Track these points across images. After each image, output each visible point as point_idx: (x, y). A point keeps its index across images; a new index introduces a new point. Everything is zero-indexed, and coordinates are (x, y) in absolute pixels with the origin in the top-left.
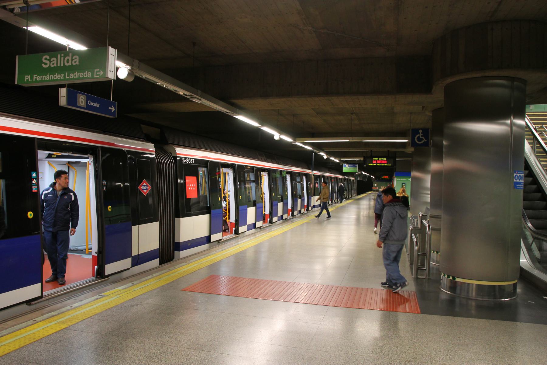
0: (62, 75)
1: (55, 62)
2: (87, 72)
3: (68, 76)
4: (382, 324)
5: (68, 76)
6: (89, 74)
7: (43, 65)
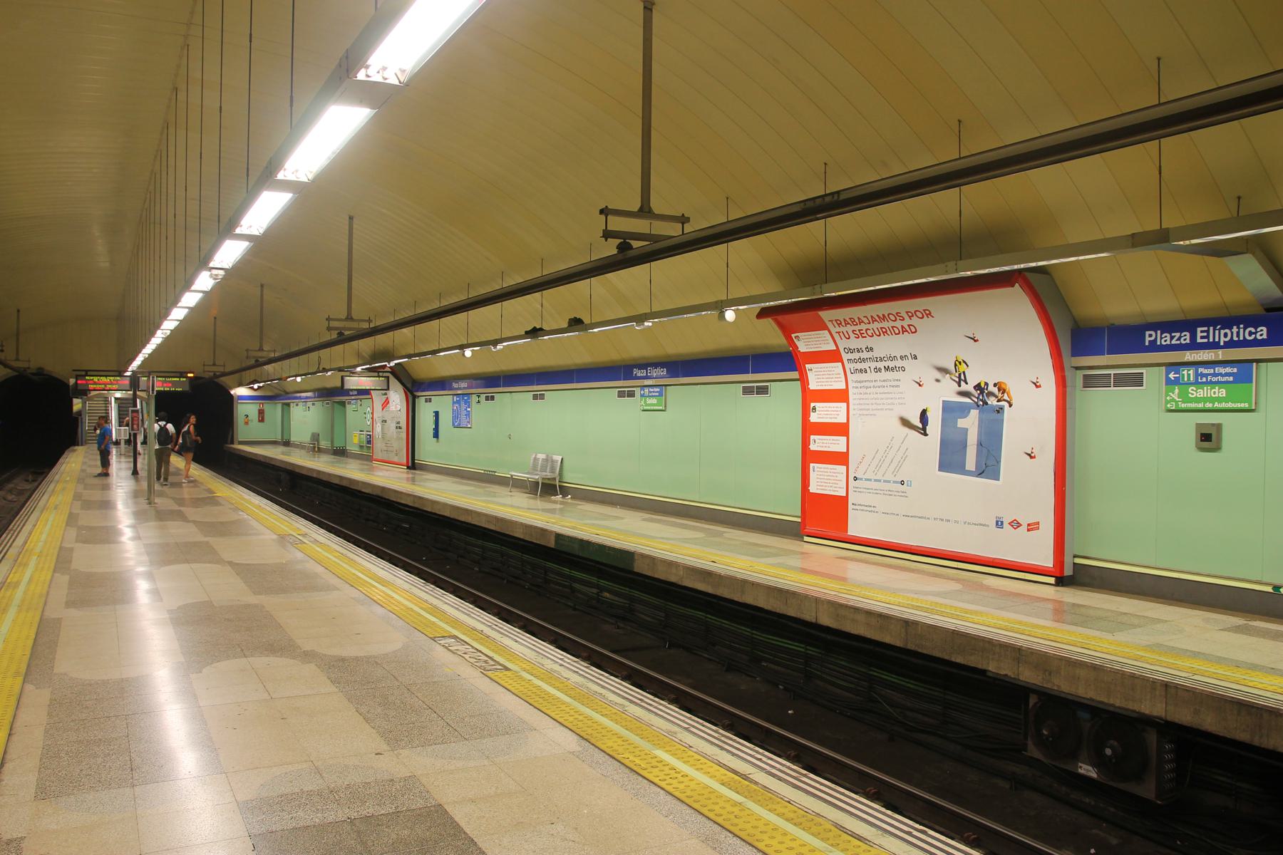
0: (1173, 334)
1: (1202, 393)
2: (1217, 388)
3: (1201, 379)
4: (126, 500)
5: (1201, 379)
6: (1166, 337)
7: (1190, 395)
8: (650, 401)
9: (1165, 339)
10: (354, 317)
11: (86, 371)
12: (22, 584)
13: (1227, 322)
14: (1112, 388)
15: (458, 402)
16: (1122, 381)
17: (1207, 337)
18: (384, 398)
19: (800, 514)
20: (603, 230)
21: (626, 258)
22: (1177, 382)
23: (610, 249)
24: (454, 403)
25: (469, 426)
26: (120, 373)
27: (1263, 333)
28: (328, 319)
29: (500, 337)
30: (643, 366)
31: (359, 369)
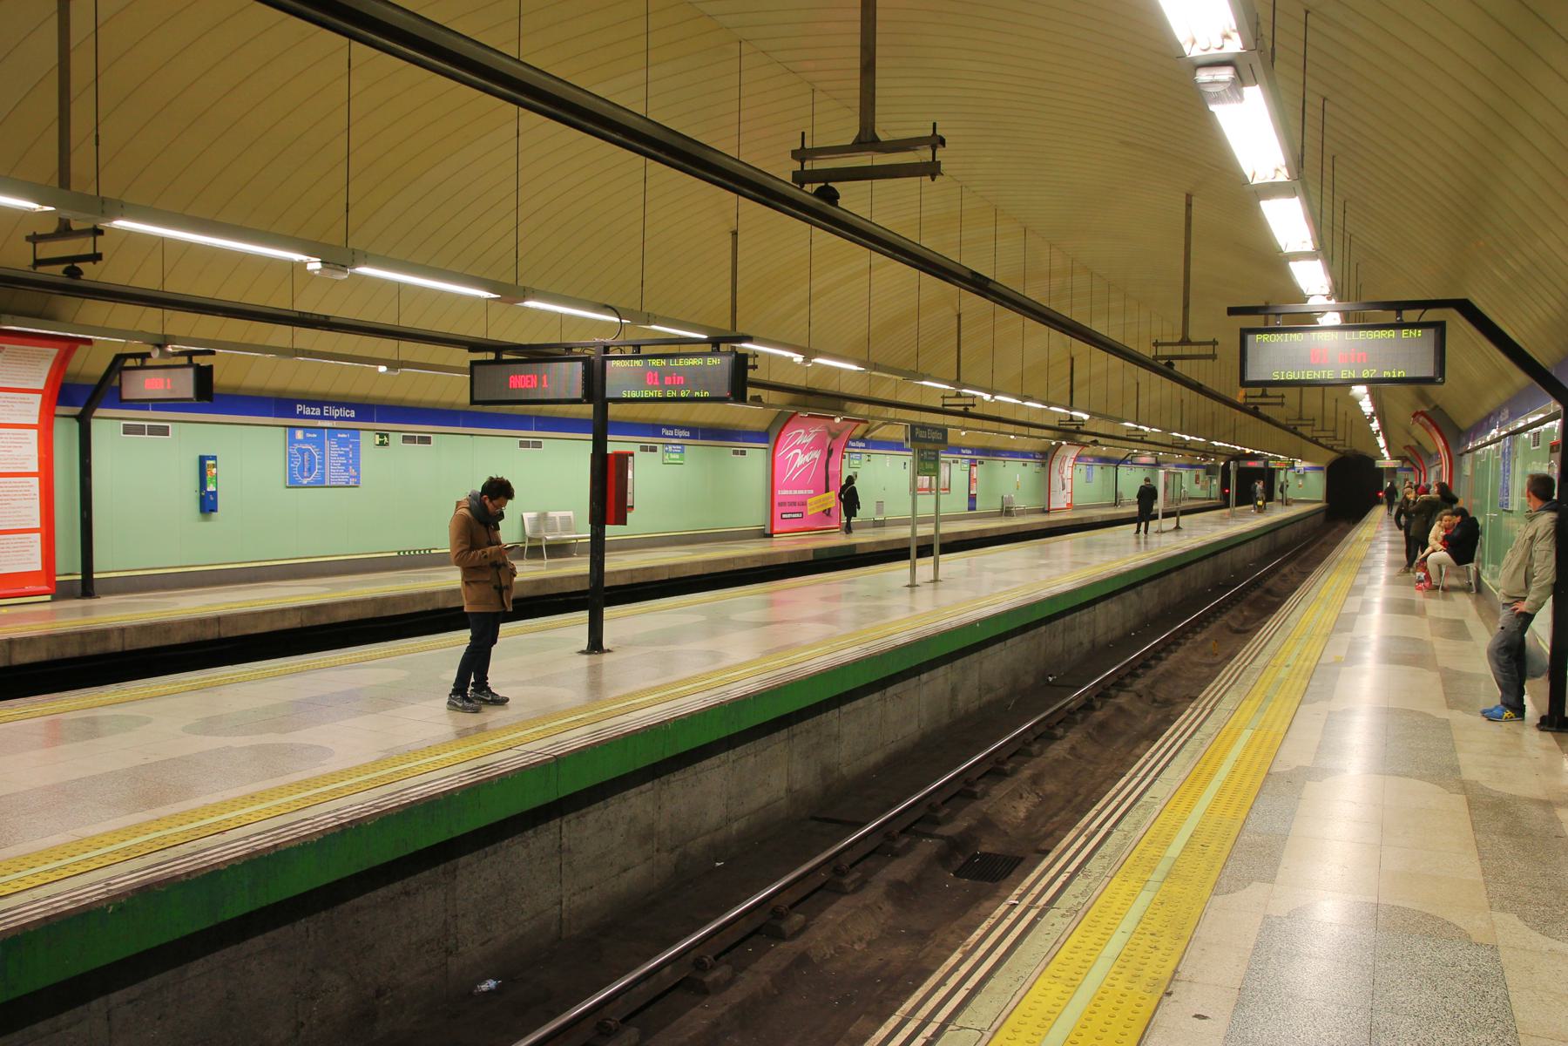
8: (673, 456)
9: (307, 411)
12: (1051, 854)
13: (338, 405)
14: (146, 436)
16: (154, 431)
17: (328, 413)
22: (667, 451)
27: (353, 414)
28: (801, 154)
30: (670, 427)
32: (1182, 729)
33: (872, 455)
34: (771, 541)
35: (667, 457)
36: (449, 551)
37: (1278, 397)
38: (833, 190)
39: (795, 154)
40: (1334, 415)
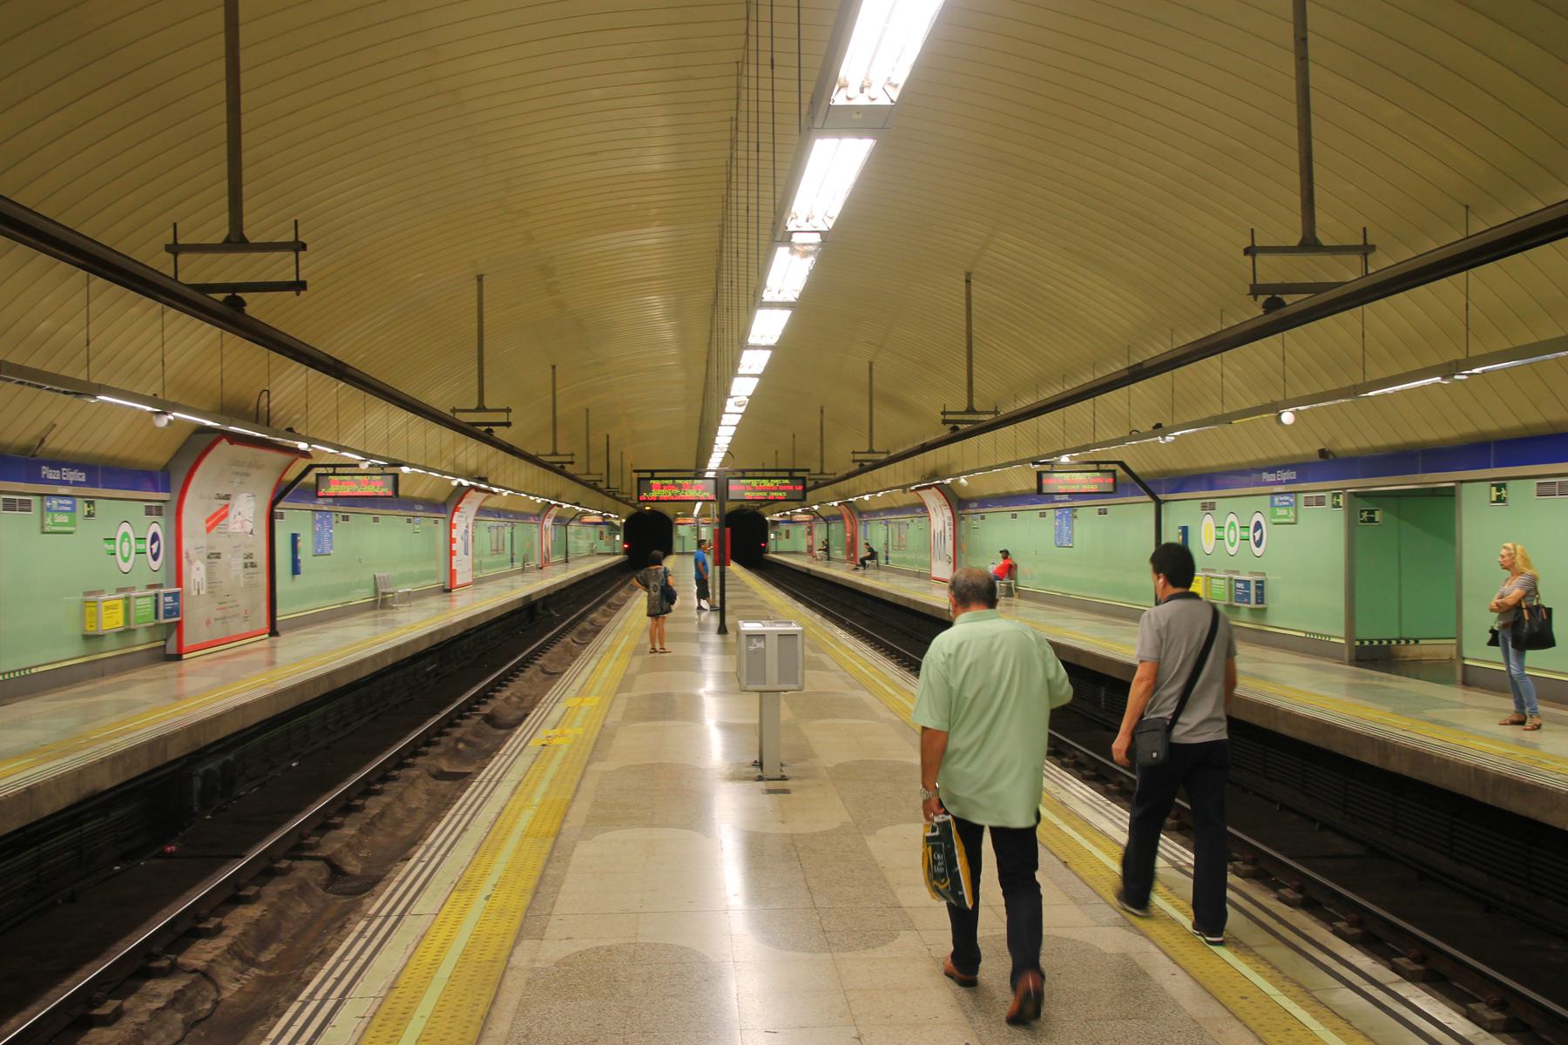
10: (1325, 240)
11: (652, 472)
15: (1060, 517)
18: (217, 505)
19: (1343, 635)
20: (1251, 285)
21: (957, 436)
22: (49, 509)
23: (856, 467)
24: (1056, 518)
25: (1070, 545)
26: (698, 473)
28: (944, 413)
29: (1361, 381)
31: (1065, 459)
32: (469, 802)
33: (97, 501)
34: (451, 596)
35: (48, 521)
36: (1343, 641)
37: (567, 455)
38: (240, 298)
39: (942, 413)
40: (620, 468)
